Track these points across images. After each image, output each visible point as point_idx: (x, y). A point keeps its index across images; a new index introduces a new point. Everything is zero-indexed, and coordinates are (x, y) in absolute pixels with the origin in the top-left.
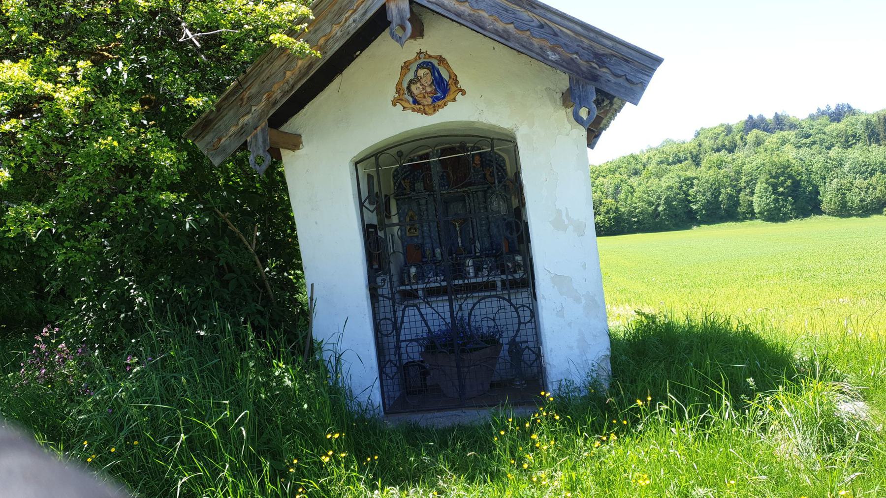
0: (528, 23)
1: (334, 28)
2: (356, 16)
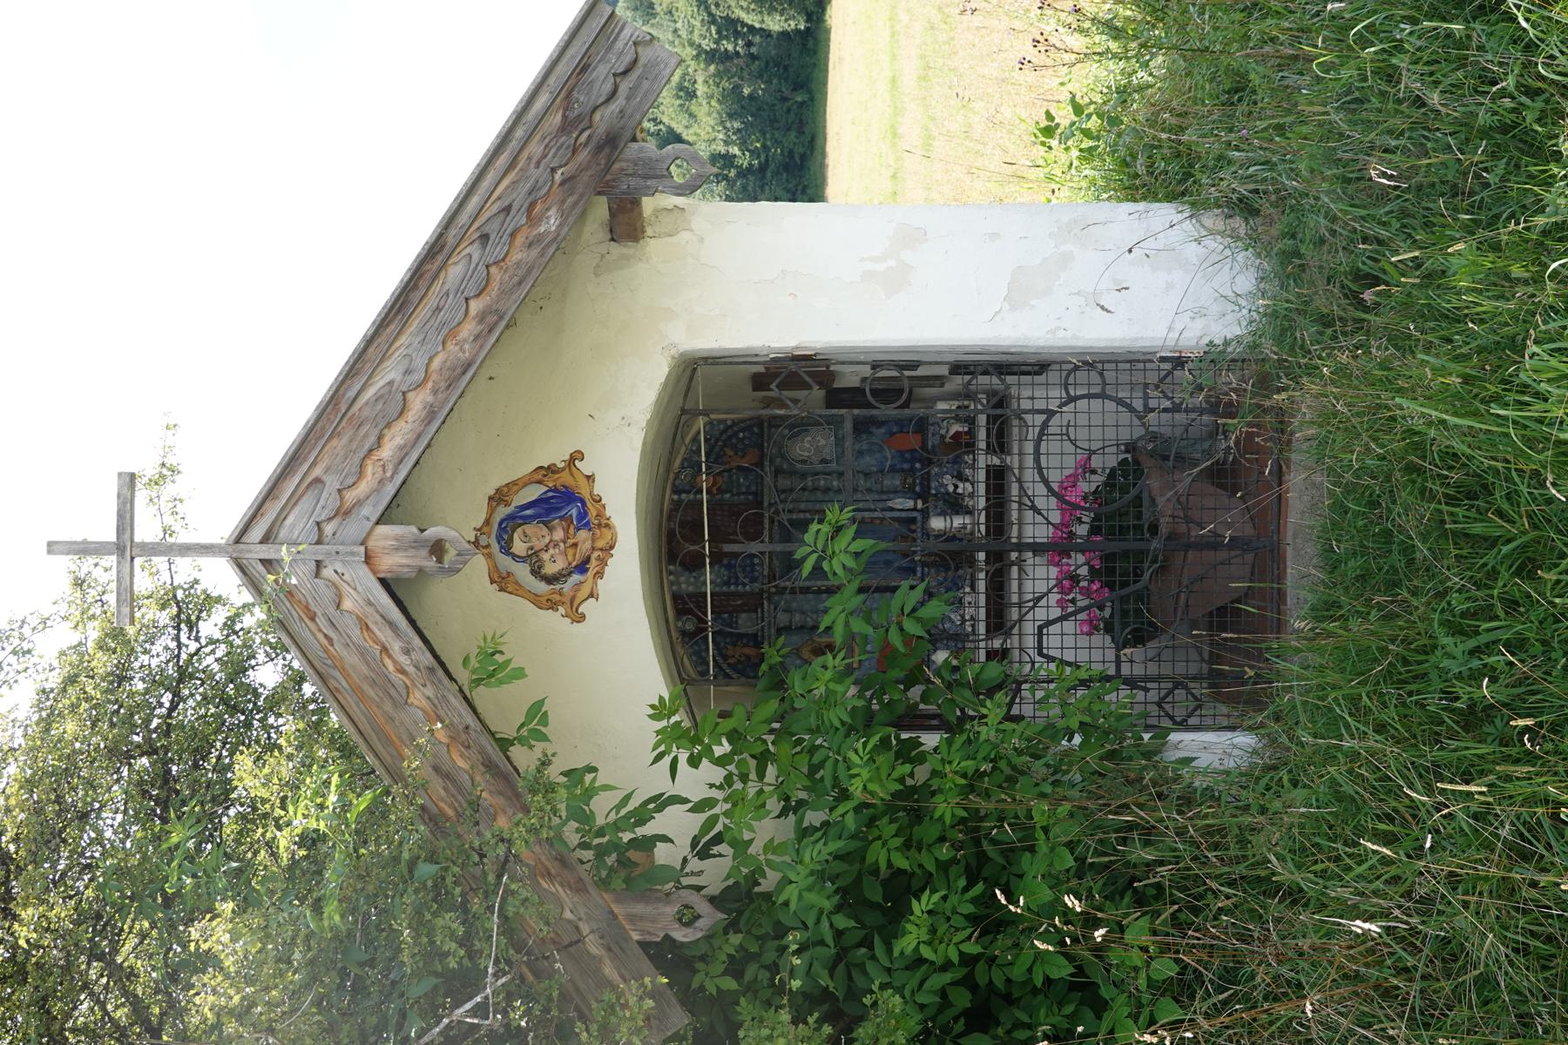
0: (473, 266)
1: (416, 703)
2: (396, 647)
